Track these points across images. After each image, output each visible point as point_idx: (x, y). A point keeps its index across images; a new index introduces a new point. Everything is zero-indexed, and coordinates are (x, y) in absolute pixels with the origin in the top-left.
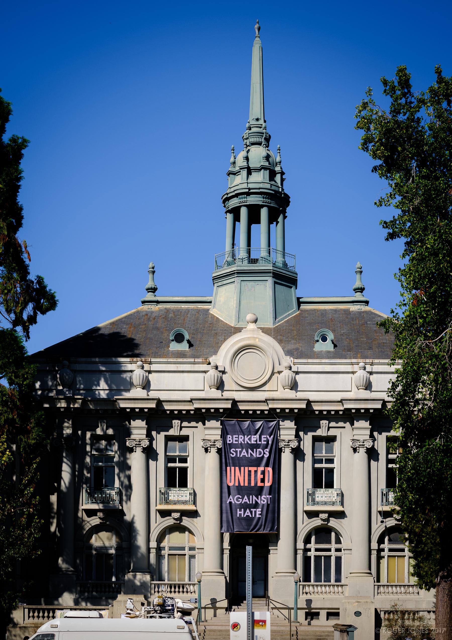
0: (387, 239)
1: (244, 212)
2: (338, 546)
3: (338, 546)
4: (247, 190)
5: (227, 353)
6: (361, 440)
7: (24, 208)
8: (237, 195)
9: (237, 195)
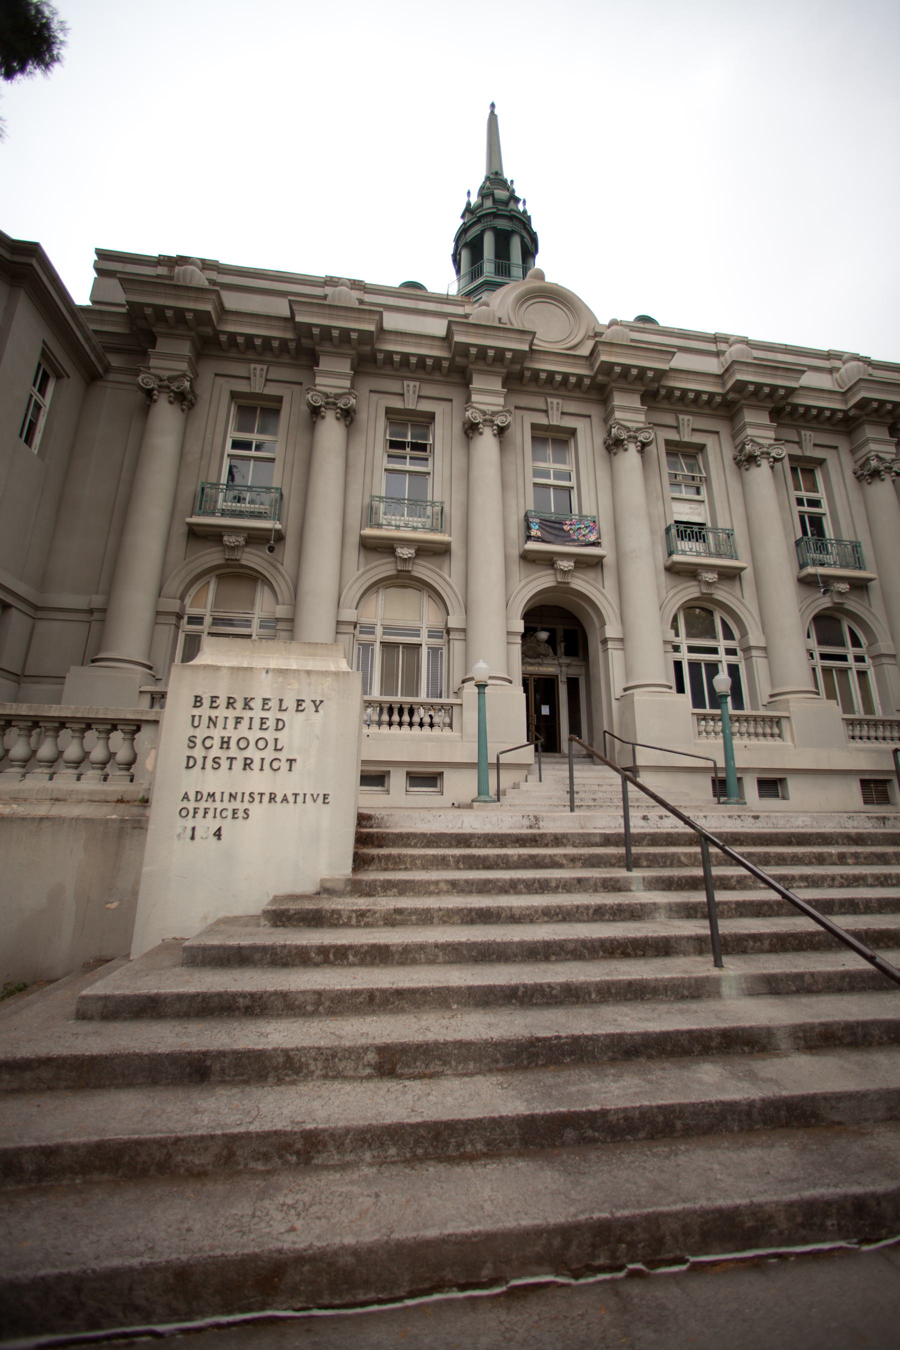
1: (489, 241)
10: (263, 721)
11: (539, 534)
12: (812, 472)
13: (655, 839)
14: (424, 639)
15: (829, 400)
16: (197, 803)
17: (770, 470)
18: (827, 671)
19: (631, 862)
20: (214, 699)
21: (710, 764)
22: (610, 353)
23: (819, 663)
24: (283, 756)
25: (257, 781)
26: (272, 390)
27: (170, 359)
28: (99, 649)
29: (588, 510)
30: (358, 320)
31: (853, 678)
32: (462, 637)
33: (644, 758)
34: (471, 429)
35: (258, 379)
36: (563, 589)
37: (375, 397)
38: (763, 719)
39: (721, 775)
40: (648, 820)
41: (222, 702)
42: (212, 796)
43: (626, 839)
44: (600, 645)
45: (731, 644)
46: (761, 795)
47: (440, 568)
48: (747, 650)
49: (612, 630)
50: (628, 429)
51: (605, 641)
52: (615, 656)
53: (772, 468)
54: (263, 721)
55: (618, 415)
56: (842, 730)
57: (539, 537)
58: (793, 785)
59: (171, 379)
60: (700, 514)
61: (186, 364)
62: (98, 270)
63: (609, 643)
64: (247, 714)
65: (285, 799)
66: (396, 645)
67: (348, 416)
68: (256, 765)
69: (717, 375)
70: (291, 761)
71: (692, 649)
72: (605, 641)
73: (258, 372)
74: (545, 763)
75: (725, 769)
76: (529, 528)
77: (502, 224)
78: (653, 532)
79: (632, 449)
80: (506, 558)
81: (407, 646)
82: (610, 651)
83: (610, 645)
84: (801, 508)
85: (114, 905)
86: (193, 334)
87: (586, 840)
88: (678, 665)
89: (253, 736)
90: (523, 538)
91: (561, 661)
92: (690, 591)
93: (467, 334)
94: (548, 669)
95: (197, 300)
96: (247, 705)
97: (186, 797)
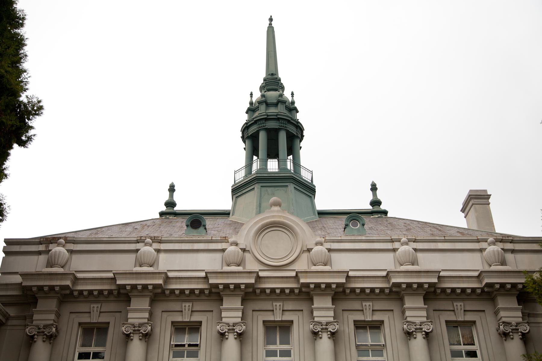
0: (173, 183)
1: (262, 137)
6: (514, 323)
8: (278, 119)
9: (278, 119)
15: (468, 282)
22: (306, 277)
26: (103, 319)
27: (44, 315)
30: (153, 278)
35: (95, 314)
55: (408, 313)
59: (46, 326)
61: (54, 315)
62: (4, 252)
67: (147, 337)
69: (383, 277)
73: (95, 309)
77: (272, 125)
79: (325, 336)
86: (59, 295)
93: (217, 278)
95: (61, 279)
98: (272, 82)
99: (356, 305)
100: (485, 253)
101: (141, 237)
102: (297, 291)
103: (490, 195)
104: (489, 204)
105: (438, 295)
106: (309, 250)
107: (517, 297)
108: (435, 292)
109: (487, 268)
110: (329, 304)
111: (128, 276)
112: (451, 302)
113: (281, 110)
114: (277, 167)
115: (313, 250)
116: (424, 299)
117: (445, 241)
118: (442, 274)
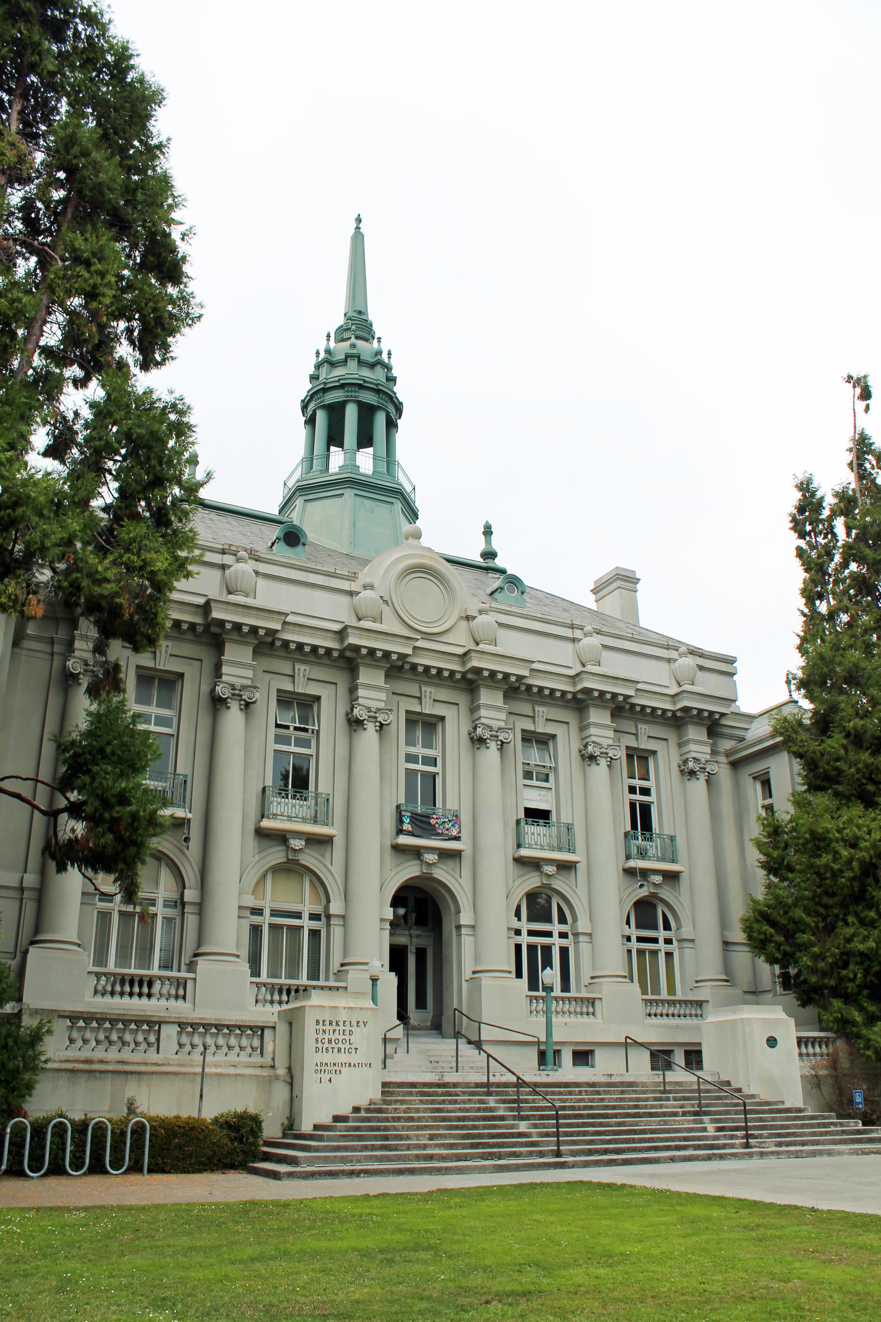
0: (487, 522)
1: (351, 414)
2: (256, 919)
3: (256, 919)
4: (362, 382)
5: (397, 561)
6: (605, 744)
7: (134, 48)
8: (342, 386)
9: (342, 386)
10: (344, 1031)
11: (410, 829)
12: (646, 759)
13: (499, 1085)
14: (307, 924)
16: (321, 1067)
17: (607, 768)
18: (641, 952)
19: (489, 1094)
20: (324, 1021)
21: (536, 1040)
22: (481, 659)
23: (634, 945)
24: (353, 1047)
25: (344, 1058)
28: (199, 945)
29: (451, 805)
31: (662, 957)
32: (342, 923)
33: (487, 1034)
34: (355, 724)
36: (428, 878)
37: (268, 677)
38: (582, 999)
39: (543, 1047)
40: (501, 1076)
41: (327, 1023)
42: (326, 1064)
43: (488, 1085)
44: (454, 929)
45: (564, 928)
46: (575, 1064)
47: (323, 856)
48: (576, 935)
49: (465, 918)
50: (490, 728)
51: (459, 927)
52: (467, 941)
53: (609, 766)
54: (344, 1031)
55: (483, 712)
56: (640, 1009)
57: (410, 832)
58: (600, 1056)
60: (547, 801)
63: (463, 929)
64: (337, 1028)
65: (355, 1065)
66: (281, 927)
68: (343, 1050)
70: (356, 1049)
71: (531, 933)
72: (459, 927)
74: (413, 1035)
75: (545, 1043)
76: (401, 822)
77: (369, 398)
78: (505, 824)
80: (382, 848)
81: (290, 928)
82: (463, 936)
83: (463, 931)
84: (633, 797)
85: (271, 1114)
87: (467, 1085)
88: (518, 947)
89: (341, 1037)
90: (394, 832)
91: (412, 932)
92: (533, 881)
94: (402, 940)
96: (337, 1024)
97: (317, 1065)
98: (358, 325)
99: (285, 667)
100: (356, 599)
101: (230, 545)
102: (335, 654)
103: (639, 580)
104: (636, 591)
105: (275, 650)
106: (468, 618)
107: (504, 693)
108: (272, 643)
109: (354, 622)
110: (704, 737)
111: (231, 608)
112: (418, 685)
113: (378, 375)
114: (371, 468)
115: (232, 568)
116: (386, 676)
117: (633, 640)
118: (290, 619)
